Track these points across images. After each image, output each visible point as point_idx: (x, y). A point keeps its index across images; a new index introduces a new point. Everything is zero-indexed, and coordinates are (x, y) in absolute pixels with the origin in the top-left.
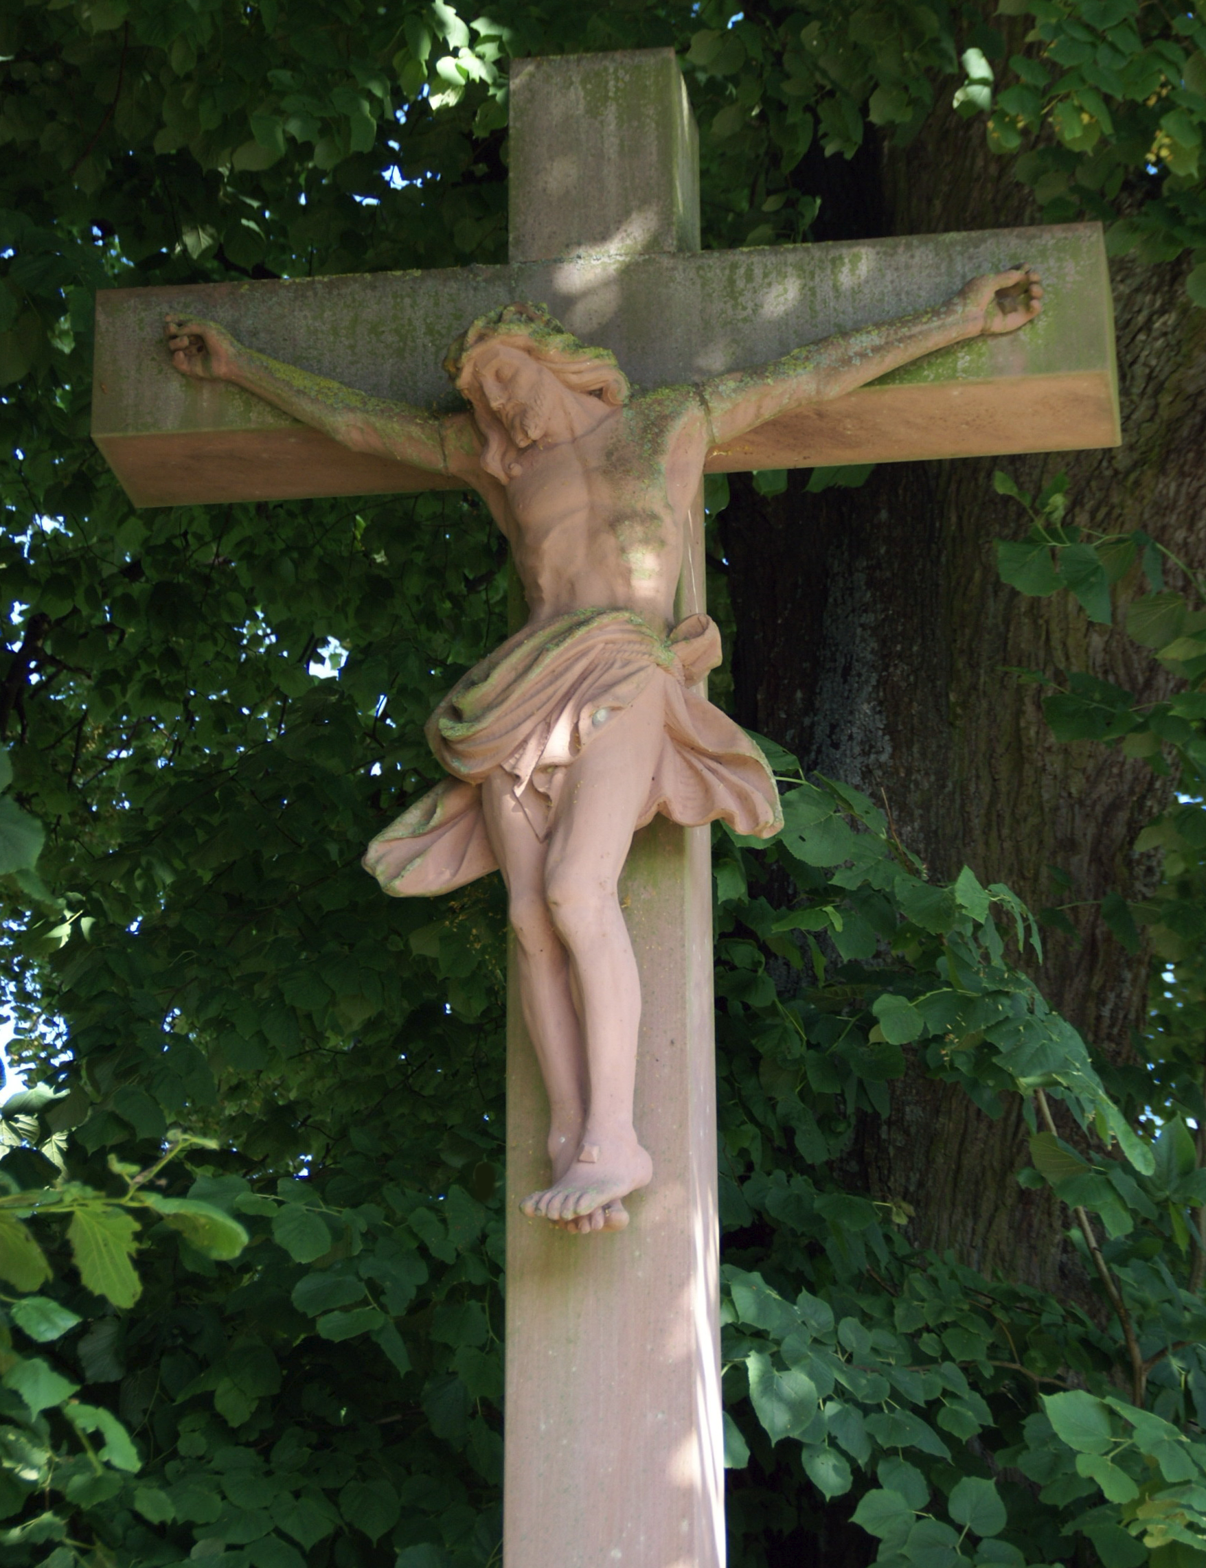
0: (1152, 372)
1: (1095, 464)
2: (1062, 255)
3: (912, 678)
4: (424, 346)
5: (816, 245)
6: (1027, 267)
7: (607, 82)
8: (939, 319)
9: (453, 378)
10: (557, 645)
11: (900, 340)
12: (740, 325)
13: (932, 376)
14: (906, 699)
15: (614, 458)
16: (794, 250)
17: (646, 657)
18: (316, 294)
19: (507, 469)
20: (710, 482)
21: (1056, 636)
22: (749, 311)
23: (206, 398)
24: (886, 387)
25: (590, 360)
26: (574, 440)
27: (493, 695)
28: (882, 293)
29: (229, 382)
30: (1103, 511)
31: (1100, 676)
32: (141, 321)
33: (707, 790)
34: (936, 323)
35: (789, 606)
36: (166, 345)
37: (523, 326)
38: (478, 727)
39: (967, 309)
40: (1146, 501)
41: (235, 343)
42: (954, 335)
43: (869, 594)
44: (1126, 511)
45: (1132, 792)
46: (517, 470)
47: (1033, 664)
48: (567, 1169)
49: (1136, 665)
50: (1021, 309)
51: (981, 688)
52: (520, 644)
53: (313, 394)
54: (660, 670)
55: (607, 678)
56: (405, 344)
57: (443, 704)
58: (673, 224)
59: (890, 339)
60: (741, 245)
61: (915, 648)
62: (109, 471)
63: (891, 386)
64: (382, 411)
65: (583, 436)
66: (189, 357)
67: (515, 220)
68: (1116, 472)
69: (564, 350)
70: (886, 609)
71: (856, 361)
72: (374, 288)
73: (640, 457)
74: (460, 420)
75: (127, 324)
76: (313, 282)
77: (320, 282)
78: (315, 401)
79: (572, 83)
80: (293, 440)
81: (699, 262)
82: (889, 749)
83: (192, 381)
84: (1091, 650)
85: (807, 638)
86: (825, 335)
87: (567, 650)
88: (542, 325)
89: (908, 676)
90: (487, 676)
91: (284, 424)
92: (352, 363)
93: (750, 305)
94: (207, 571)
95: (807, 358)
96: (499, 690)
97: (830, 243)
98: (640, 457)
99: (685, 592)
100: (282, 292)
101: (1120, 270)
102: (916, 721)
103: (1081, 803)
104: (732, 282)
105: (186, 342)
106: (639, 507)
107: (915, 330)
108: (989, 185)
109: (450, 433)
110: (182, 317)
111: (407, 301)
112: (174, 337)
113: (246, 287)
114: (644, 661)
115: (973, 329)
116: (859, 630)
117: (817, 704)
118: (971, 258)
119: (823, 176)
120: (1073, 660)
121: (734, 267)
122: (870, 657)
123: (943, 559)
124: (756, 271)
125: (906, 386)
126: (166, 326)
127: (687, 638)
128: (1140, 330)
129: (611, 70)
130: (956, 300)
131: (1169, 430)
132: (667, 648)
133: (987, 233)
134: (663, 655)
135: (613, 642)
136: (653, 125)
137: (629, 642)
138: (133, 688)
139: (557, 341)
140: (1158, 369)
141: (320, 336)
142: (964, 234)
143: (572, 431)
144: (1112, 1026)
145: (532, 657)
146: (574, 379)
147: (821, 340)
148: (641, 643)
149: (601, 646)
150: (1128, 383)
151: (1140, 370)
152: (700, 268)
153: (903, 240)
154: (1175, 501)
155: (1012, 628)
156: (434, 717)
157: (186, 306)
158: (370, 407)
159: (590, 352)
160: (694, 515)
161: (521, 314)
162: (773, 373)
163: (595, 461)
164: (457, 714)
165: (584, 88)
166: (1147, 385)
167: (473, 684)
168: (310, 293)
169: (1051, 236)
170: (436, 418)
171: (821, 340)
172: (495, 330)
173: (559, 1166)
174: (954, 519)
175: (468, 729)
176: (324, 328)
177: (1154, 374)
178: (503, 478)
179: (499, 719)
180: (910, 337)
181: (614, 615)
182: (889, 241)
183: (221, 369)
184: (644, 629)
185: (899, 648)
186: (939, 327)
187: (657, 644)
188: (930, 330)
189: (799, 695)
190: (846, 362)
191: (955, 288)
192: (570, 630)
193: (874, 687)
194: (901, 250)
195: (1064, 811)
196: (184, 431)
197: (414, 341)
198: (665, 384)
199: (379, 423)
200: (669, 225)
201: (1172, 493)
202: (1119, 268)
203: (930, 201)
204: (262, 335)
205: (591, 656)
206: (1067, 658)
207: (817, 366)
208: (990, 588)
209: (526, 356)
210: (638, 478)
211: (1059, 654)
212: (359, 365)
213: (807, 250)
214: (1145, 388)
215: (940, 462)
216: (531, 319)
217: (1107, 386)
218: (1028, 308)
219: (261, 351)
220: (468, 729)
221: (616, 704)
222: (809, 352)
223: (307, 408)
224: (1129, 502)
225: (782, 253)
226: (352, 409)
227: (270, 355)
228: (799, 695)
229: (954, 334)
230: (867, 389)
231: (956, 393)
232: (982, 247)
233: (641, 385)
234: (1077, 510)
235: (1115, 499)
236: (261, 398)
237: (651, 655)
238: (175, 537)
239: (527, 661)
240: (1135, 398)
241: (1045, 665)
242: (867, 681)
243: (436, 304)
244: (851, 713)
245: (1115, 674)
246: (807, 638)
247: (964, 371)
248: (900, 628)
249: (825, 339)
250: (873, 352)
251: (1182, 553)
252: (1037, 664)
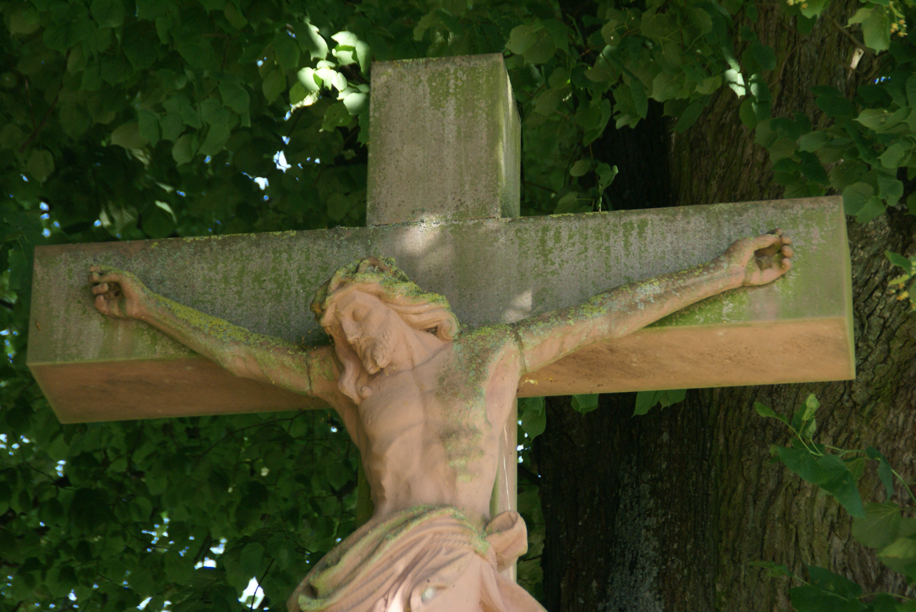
0: (885, 322)
1: (838, 398)
2: (810, 222)
3: (686, 571)
4: (297, 292)
5: (611, 213)
6: (781, 231)
7: (448, 81)
8: (709, 273)
9: (318, 317)
10: (395, 535)
11: (677, 290)
12: (549, 277)
13: (702, 320)
14: (681, 589)
15: (445, 383)
16: (594, 216)
17: (466, 545)
18: (211, 250)
19: (359, 392)
20: (523, 405)
21: (804, 539)
22: (557, 265)
23: (121, 334)
24: (665, 328)
25: (428, 303)
26: (414, 368)
27: (342, 576)
28: (664, 252)
29: (139, 320)
30: (844, 436)
31: (840, 572)
32: (70, 270)
34: (706, 276)
35: (588, 510)
36: (90, 291)
37: (375, 276)
38: (330, 602)
39: (732, 265)
40: (879, 429)
41: (146, 288)
42: (720, 286)
43: (652, 502)
44: (862, 436)
46: (367, 392)
47: (785, 562)
49: (870, 565)
50: (775, 266)
51: (742, 580)
52: (365, 534)
53: (206, 330)
54: (477, 557)
55: (435, 562)
56: (282, 290)
57: (303, 584)
58: (497, 195)
59: (669, 289)
60: (552, 213)
61: (689, 547)
62: (43, 397)
63: (669, 327)
64: (261, 344)
65: (421, 365)
66: (108, 300)
67: (372, 191)
68: (855, 404)
69: (407, 295)
70: (665, 514)
71: (641, 307)
72: (258, 245)
73: (466, 382)
74: (324, 351)
75: (59, 274)
76: (210, 240)
77: (215, 240)
78: (207, 336)
79: (420, 81)
80: (189, 368)
81: (517, 226)
83: (110, 320)
84: (832, 551)
85: (602, 537)
86: (617, 285)
87: (403, 539)
88: (390, 275)
89: (683, 569)
90: (338, 560)
91: (183, 355)
92: (239, 305)
93: (558, 261)
94: (119, 479)
95: (601, 304)
96: (347, 571)
97: (623, 211)
98: (466, 382)
99: (499, 493)
100: (185, 248)
101: (862, 238)
102: (688, 606)
104: (543, 242)
105: (106, 287)
106: (464, 423)
107: (689, 282)
108: (756, 169)
109: (315, 363)
110: (103, 268)
111: (285, 256)
112: (97, 284)
113: (156, 243)
114: (465, 549)
115: (736, 282)
116: (644, 531)
117: (609, 592)
118: (735, 224)
119: (621, 159)
120: (817, 559)
121: (545, 230)
122: (652, 553)
123: (713, 474)
124: (563, 233)
125: (681, 327)
126: (90, 275)
127: (501, 529)
128: (877, 288)
129: (452, 71)
130: (722, 258)
131: (899, 370)
132: (484, 538)
133: (749, 204)
134: (480, 544)
135: (441, 533)
136: (484, 116)
137: (453, 533)
138: (53, 572)
139: (403, 287)
140: (890, 320)
141: (214, 283)
142: (731, 204)
143: (412, 361)
145: (374, 545)
146: (415, 319)
147: (613, 289)
148: (462, 534)
149: (431, 536)
150: (865, 331)
151: (875, 321)
152: (519, 230)
153: (681, 209)
154: (903, 429)
155: (768, 532)
156: (294, 594)
157: (107, 259)
158: (251, 340)
159: (428, 297)
160: (509, 432)
161: (374, 266)
162: (574, 315)
163: (429, 386)
164: (313, 592)
165: (430, 86)
166: (881, 332)
167: (327, 567)
168: (207, 249)
169: (802, 207)
170: (304, 350)
171: (613, 289)
172: (353, 279)
174: (722, 440)
175: (321, 604)
176: (217, 277)
177: (887, 325)
178: (356, 399)
179: (346, 596)
180: (685, 288)
181: (442, 511)
182: (670, 210)
184: (465, 523)
185: (675, 546)
186: (708, 280)
187: (475, 536)
188: (701, 282)
189: (594, 584)
190: (633, 307)
191: (722, 248)
192: (406, 523)
193: (655, 578)
194: (679, 217)
196: (102, 360)
197: (288, 288)
198: (488, 323)
199: (258, 354)
200: (494, 196)
201: (900, 423)
202: (856, 231)
203: (707, 182)
204: (168, 282)
205: (422, 544)
206: (813, 557)
207: (609, 310)
208: (750, 498)
209: (377, 300)
210: (464, 399)
211: (806, 553)
212: (244, 308)
213: (604, 216)
214: (880, 335)
215: (711, 390)
216: (381, 270)
217: (844, 329)
218: (781, 264)
219: (166, 295)
220: (321, 604)
221: (441, 584)
222: (604, 298)
223: (201, 342)
224: (866, 429)
225: (584, 219)
226: (237, 343)
227: (173, 299)
228: (594, 584)
229: (720, 286)
230: (649, 329)
231: (721, 334)
232: (745, 216)
233: (468, 325)
234: (822, 435)
235: (854, 427)
236: (164, 334)
237: (470, 544)
238: (96, 451)
239: (371, 549)
240: (871, 343)
241: (795, 563)
242: (649, 574)
243: (307, 259)
244: (636, 599)
245: (852, 571)
246: (602, 537)
247: (728, 316)
248: (677, 530)
249: (617, 289)
250: (652, 298)
251: (909, 473)
252: (788, 561)
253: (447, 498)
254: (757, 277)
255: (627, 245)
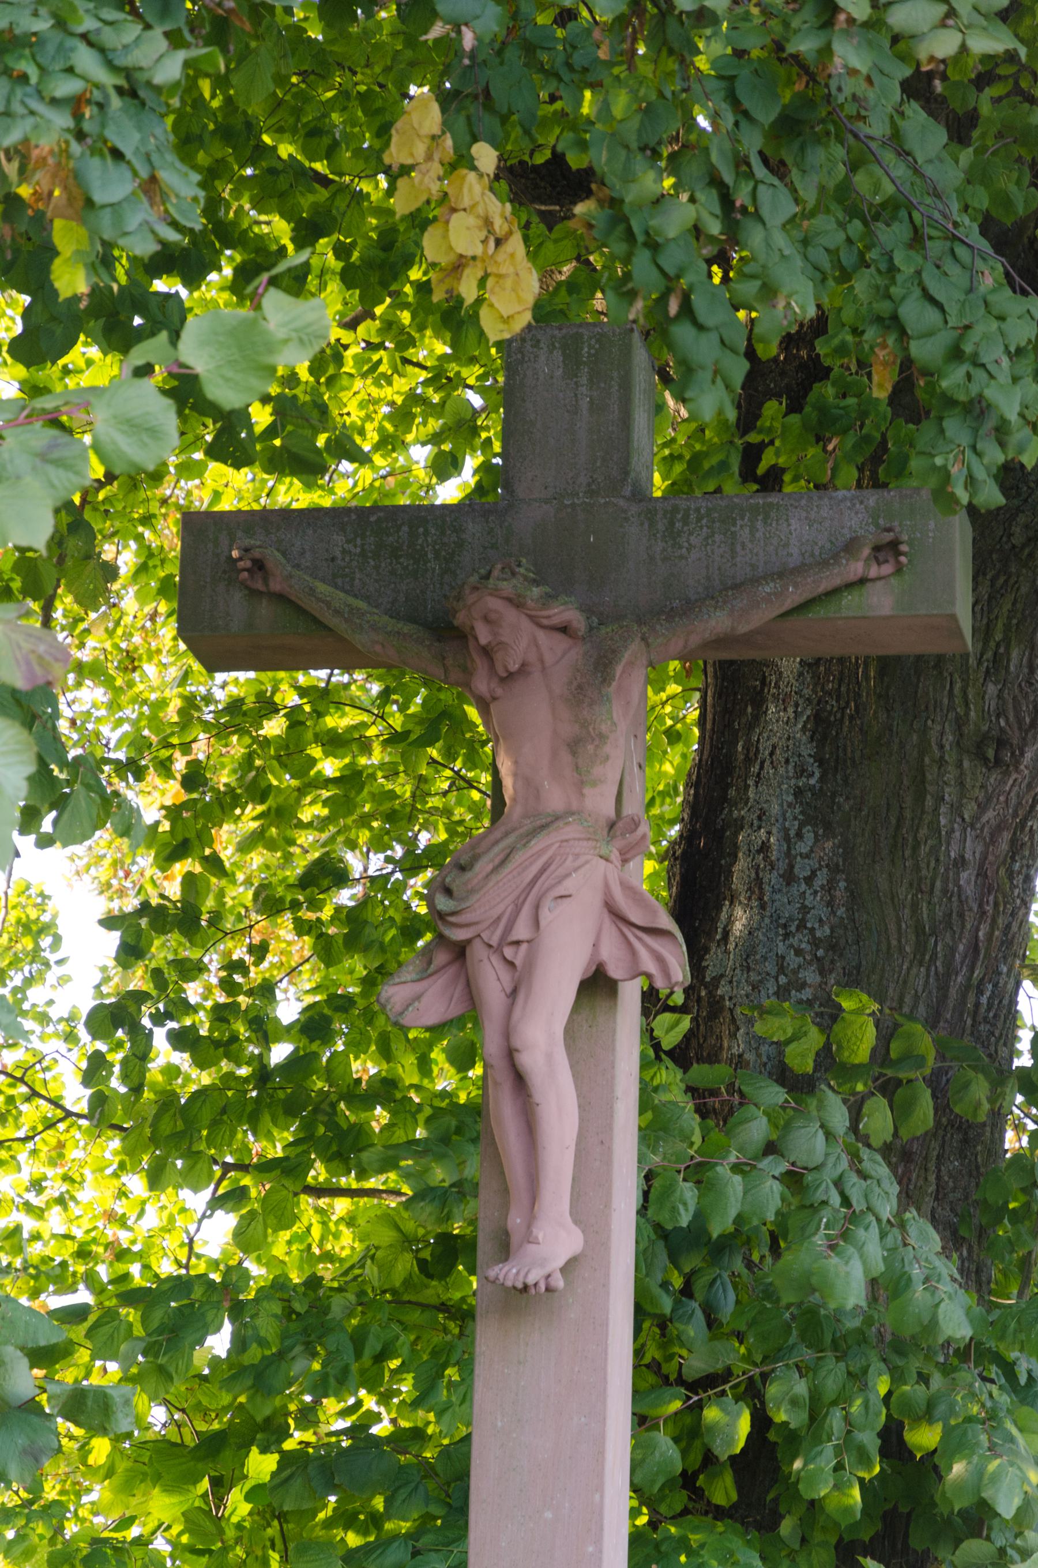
30: (1001, 580)
33: (633, 952)
45: (1015, 815)
48: (520, 1246)
55: (561, 871)
68: (1014, 547)
82: (817, 775)
83: (254, 593)
99: (627, 779)
103: (972, 826)
144: (989, 1010)
146: (545, 622)
173: (515, 1240)
183: (275, 586)
195: (957, 834)
205: (550, 853)
253: (575, 805)
254: (874, 571)
255: (752, 533)
